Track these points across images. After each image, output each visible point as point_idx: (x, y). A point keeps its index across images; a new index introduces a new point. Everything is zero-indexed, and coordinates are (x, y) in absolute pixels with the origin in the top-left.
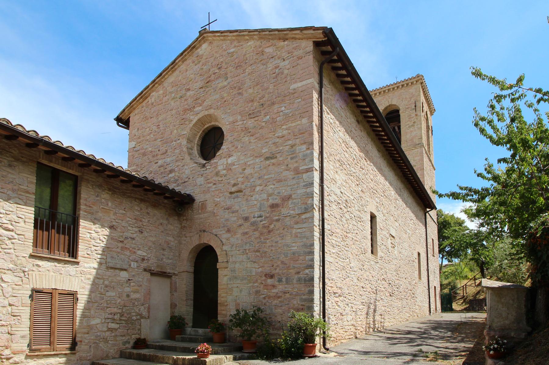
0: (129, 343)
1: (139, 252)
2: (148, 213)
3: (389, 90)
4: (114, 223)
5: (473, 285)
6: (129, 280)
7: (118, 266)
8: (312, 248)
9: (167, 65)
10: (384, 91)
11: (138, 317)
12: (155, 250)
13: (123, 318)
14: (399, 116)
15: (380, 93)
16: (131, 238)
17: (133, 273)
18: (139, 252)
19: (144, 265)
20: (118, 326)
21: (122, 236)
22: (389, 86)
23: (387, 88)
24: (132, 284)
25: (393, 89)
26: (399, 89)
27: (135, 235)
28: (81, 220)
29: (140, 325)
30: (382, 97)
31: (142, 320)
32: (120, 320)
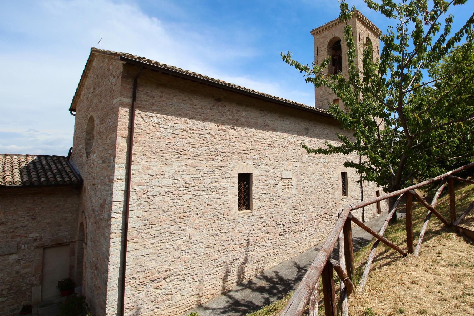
0: (18, 309)
1: (32, 235)
2: (42, 202)
3: (332, 25)
4: (3, 220)
5: (357, 214)
6: (19, 260)
7: (6, 253)
8: (106, 274)
9: (115, 50)
10: (329, 27)
11: (29, 286)
12: (49, 229)
13: (11, 292)
14: (341, 45)
15: (326, 28)
16: (22, 227)
17: (24, 254)
18: (32, 235)
19: (37, 243)
20: (6, 298)
21: (12, 228)
22: (332, 22)
23: (331, 24)
24: (22, 263)
25: (336, 24)
26: (340, 24)
27: (26, 224)
28: (136, 112)
29: (31, 292)
30: (328, 32)
31: (33, 288)
32: (8, 293)
